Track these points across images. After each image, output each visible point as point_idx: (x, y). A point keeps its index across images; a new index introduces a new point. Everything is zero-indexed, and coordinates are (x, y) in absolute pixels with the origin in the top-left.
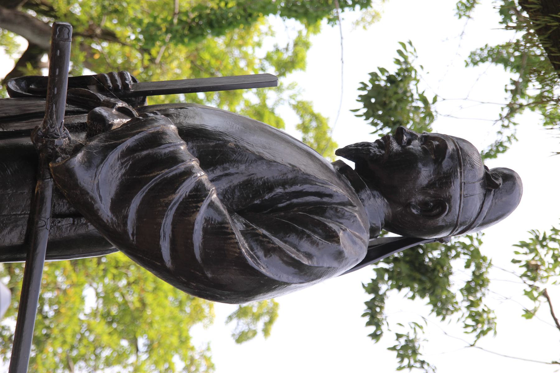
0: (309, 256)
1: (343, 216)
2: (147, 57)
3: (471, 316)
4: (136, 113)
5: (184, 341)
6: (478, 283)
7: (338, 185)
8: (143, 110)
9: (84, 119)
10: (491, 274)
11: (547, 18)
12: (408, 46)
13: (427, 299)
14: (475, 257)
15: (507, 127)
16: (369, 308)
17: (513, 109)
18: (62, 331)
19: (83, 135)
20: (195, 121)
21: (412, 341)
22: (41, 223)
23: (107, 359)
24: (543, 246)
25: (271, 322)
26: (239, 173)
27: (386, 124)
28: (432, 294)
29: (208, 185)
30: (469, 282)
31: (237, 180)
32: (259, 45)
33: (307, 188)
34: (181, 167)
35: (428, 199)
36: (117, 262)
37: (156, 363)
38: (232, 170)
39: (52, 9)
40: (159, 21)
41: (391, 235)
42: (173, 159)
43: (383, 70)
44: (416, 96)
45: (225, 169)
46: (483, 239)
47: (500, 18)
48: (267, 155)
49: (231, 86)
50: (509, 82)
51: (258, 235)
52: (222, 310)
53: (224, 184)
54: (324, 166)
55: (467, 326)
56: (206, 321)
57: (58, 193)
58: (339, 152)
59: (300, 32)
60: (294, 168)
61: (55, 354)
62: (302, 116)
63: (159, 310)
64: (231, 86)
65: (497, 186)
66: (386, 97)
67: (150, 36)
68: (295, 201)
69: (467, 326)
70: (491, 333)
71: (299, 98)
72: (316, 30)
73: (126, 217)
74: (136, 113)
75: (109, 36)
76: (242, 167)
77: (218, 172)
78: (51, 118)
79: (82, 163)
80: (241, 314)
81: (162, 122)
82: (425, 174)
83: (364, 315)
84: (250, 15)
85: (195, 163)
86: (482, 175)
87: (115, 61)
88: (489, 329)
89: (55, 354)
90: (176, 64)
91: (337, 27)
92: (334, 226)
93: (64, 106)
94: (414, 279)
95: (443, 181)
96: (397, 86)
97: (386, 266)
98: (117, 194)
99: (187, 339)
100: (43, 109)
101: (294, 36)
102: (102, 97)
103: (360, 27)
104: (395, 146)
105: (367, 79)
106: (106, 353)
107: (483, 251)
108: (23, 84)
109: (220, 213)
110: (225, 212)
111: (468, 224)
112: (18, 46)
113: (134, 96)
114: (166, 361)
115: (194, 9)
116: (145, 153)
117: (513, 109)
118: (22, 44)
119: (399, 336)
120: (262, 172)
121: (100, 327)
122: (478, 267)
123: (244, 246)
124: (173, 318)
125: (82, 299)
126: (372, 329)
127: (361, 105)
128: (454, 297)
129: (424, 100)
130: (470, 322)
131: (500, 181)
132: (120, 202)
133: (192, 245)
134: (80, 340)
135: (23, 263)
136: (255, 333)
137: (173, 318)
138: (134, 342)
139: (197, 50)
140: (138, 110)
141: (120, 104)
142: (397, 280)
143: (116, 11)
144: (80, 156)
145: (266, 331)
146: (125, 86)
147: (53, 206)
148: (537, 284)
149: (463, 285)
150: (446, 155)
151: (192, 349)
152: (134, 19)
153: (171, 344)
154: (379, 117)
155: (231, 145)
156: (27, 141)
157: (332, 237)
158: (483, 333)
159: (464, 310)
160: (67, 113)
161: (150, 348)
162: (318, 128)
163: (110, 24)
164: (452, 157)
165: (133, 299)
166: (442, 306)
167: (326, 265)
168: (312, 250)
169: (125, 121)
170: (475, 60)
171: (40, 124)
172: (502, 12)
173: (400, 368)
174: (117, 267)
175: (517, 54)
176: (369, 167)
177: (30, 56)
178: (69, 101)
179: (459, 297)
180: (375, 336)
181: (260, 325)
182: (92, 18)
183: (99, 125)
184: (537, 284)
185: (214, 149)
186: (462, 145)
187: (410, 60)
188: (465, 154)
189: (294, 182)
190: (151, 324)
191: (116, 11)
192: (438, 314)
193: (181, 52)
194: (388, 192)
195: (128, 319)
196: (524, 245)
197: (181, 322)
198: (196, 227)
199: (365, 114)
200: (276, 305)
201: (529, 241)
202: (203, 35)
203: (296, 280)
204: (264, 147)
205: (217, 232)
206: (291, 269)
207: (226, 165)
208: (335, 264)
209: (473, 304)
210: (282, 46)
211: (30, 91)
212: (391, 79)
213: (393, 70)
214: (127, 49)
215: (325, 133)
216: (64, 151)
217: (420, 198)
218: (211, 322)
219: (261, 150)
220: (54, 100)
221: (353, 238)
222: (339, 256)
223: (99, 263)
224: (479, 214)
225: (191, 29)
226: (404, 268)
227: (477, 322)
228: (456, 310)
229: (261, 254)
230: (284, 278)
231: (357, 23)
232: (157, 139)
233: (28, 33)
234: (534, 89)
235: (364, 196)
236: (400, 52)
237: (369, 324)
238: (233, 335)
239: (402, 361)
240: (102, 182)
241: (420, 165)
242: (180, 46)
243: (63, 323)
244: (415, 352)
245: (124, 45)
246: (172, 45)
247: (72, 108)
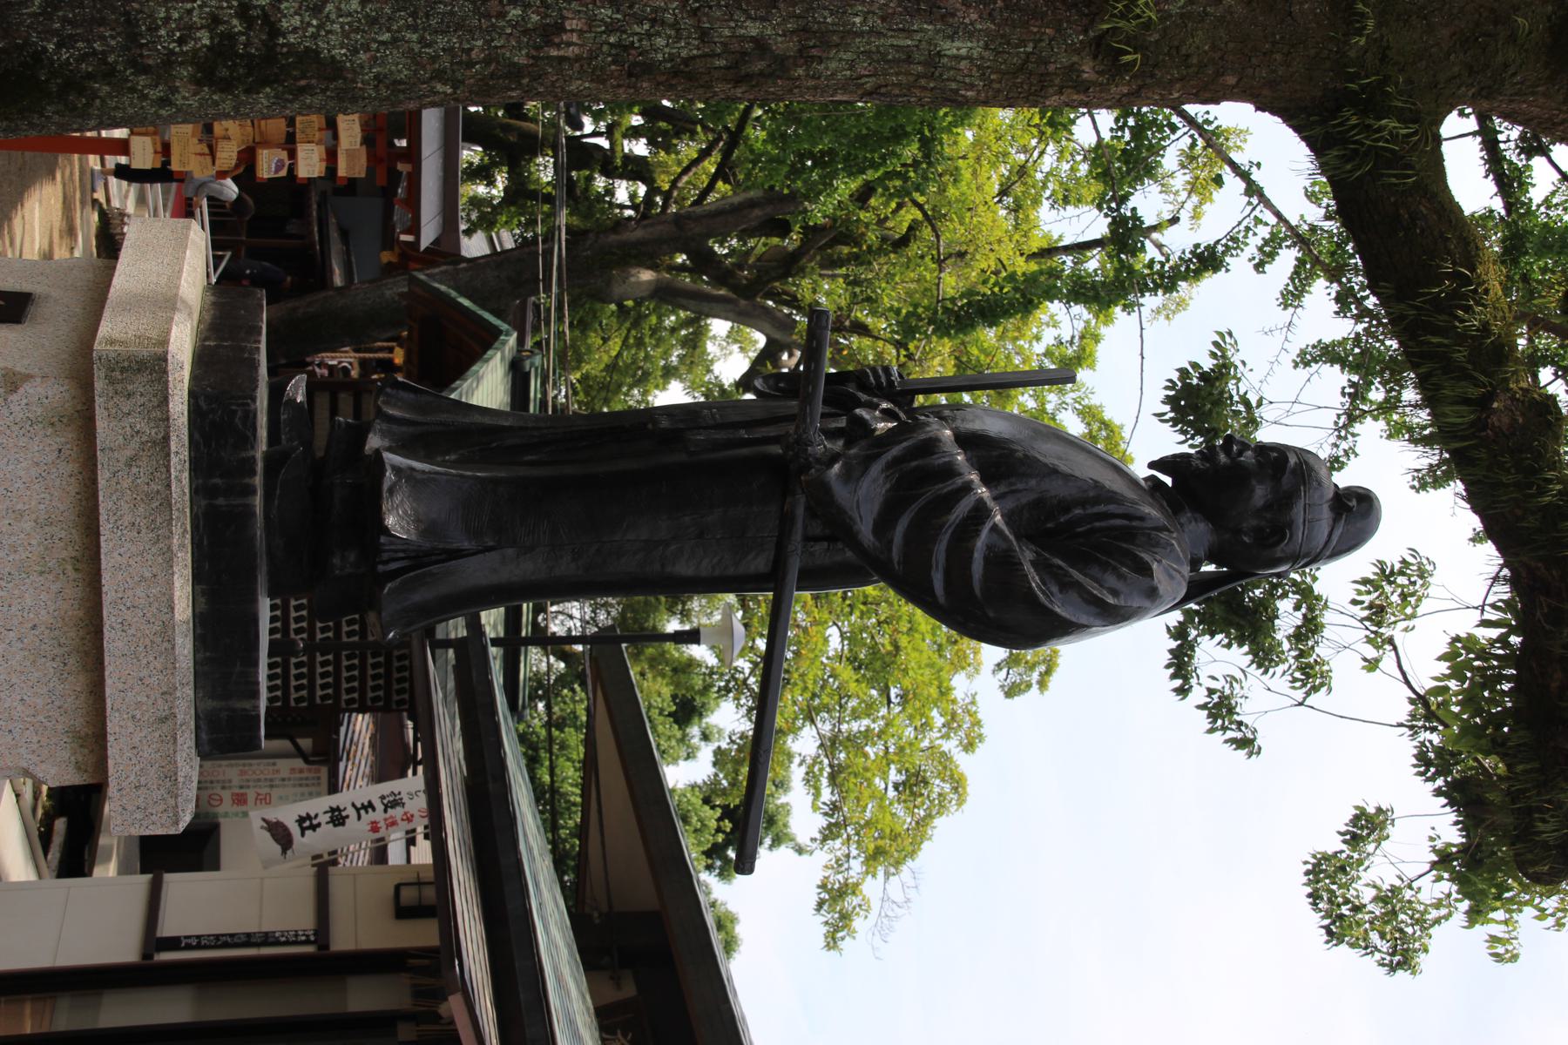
0: (1115, 593)
1: (1157, 544)
2: (903, 352)
3: (1299, 669)
4: (902, 415)
5: (944, 692)
6: (1310, 628)
7: (1151, 505)
8: (911, 412)
9: (842, 423)
10: (1328, 617)
11: (1402, 306)
12: (1228, 339)
13: (1246, 648)
14: (1307, 597)
15: (1345, 438)
16: (1175, 657)
17: (1352, 417)
18: (802, 675)
19: (841, 443)
20: (976, 426)
21: (1228, 698)
22: (791, 548)
23: (854, 710)
24: (1390, 583)
25: (1048, 672)
26: (1030, 489)
27: (1198, 432)
28: (1252, 642)
29: (990, 504)
30: (1298, 627)
31: (1025, 499)
32: (1038, 338)
33: (1112, 508)
34: (959, 481)
35: (1263, 523)
36: (866, 596)
37: (911, 718)
38: (1020, 486)
39: (795, 298)
40: (920, 310)
41: (1211, 568)
42: (950, 471)
43: (1195, 365)
44: (1236, 398)
45: (1011, 484)
46: (1318, 574)
47: (1336, 308)
48: (1063, 468)
49: (1005, 384)
50: (1346, 384)
51: (1052, 566)
52: (992, 653)
53: (1010, 503)
54: (1132, 481)
55: (1295, 680)
56: (970, 669)
57: (811, 512)
58: (1152, 465)
59: (1087, 322)
60: (1097, 484)
61: (794, 703)
62: (1088, 424)
63: (914, 655)
64: (1005, 384)
65: (1350, 509)
66: (1200, 397)
67: (908, 328)
68: (1097, 524)
69: (1295, 680)
70: (1324, 689)
71: (1086, 402)
72: (1109, 320)
73: (891, 542)
74: (902, 415)
75: (861, 329)
76: (1033, 482)
77: (1002, 489)
78: (804, 421)
79: (839, 476)
80: (1011, 662)
81: (935, 426)
82: (1261, 493)
83: (1168, 667)
84: (1031, 301)
85: (974, 477)
86: (1331, 495)
87: (866, 357)
88: (1322, 685)
89: (794, 703)
90: (938, 360)
91: (1135, 315)
92: (1146, 557)
93: (820, 408)
94: (1231, 624)
95: (1283, 502)
96: (1213, 386)
97: (1195, 607)
98: (880, 514)
99: (949, 689)
100: (796, 411)
101: (1080, 326)
102: (864, 397)
103: (1162, 318)
104: (1222, 457)
105: (1175, 376)
106: (853, 703)
107: (1318, 588)
108: (771, 382)
109: (1005, 538)
110: (1011, 537)
111: (1313, 554)
112: (756, 342)
113: (902, 394)
114: (922, 715)
115: (962, 296)
116: (914, 464)
117: (1352, 417)
118: (761, 340)
119: (1211, 692)
120: (1056, 489)
121: (847, 673)
122: (1311, 609)
123: (1035, 580)
124: (931, 665)
125: (826, 640)
126: (1178, 683)
127: (1167, 408)
128: (1280, 644)
129: (1247, 403)
130: (1298, 675)
131: (1354, 503)
132: (883, 525)
133: (971, 577)
134: (823, 688)
135: (770, 594)
136: (1029, 686)
137: (931, 665)
138: (885, 692)
139: (963, 343)
140: (905, 413)
141: (884, 405)
142: (1210, 624)
143: (869, 299)
144: (837, 467)
145: (1042, 684)
146: (890, 383)
147: (805, 528)
148: (1382, 630)
149: (1291, 631)
150: (1288, 470)
151: (954, 701)
152: (891, 309)
153: (929, 695)
154: (1190, 424)
155: (1020, 454)
156: (777, 450)
157: (1145, 570)
158: (1315, 689)
159: (1292, 661)
160: (823, 416)
161: (904, 698)
162: (1107, 438)
163: (861, 314)
164: (1294, 471)
165: (885, 642)
166: (1264, 657)
167: (1135, 605)
168: (1118, 585)
169: (890, 425)
170: (1305, 359)
171: (791, 429)
172: (1338, 299)
173: (1211, 731)
174: (864, 603)
175: (1357, 350)
176: (1187, 483)
177: (769, 354)
178: (825, 402)
179: (1286, 646)
180: (1183, 692)
181: (1035, 676)
182: (840, 309)
183: (860, 429)
184: (1382, 630)
185: (998, 459)
186: (1307, 457)
187: (1229, 354)
188: (1310, 469)
189: (1097, 501)
190: (905, 671)
191: (869, 299)
192: (1259, 666)
193: (946, 346)
194: (1213, 515)
195: (878, 664)
196: (1365, 582)
197: (941, 670)
198: (976, 555)
199: (1171, 419)
200: (1056, 652)
201: (1372, 577)
202: (973, 326)
203: (1098, 622)
204: (1060, 458)
205: (1002, 562)
206: (1093, 609)
207: (1013, 480)
208: (1147, 604)
209: (1302, 654)
210: (1066, 337)
211: (779, 389)
212: (1204, 376)
213: (1207, 364)
214: (880, 343)
215: (1117, 445)
216: (818, 461)
217: (1254, 522)
218: (977, 671)
219: (1056, 462)
220: (808, 400)
221: (1170, 575)
222: (1152, 594)
223: (844, 598)
224: (1327, 542)
225: (958, 318)
226: (1218, 610)
227: (1308, 676)
228: (1283, 661)
229: (1055, 589)
230: (1083, 620)
231: (1158, 311)
232: (931, 445)
233: (767, 326)
234: (1377, 394)
235: (1183, 520)
236: (1216, 344)
237: (1174, 677)
238: (1002, 687)
239: (1215, 721)
240: (864, 498)
241: (1254, 482)
242: (946, 340)
243: (804, 666)
244: (1231, 711)
245: (877, 338)
246: (934, 338)
247: (827, 410)
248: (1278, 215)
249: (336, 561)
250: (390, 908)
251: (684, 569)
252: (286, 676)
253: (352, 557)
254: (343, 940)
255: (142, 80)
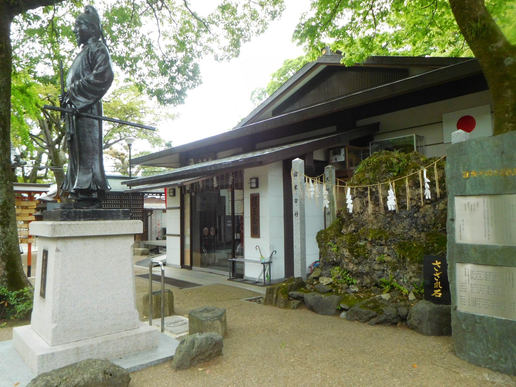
54: (82, 51)
183: (70, 102)
248: (190, 10)
249: (94, 197)
250: (174, 197)
251: (97, 136)
252: (139, 217)
253: (94, 194)
254: (179, 205)
255: (7, 237)
